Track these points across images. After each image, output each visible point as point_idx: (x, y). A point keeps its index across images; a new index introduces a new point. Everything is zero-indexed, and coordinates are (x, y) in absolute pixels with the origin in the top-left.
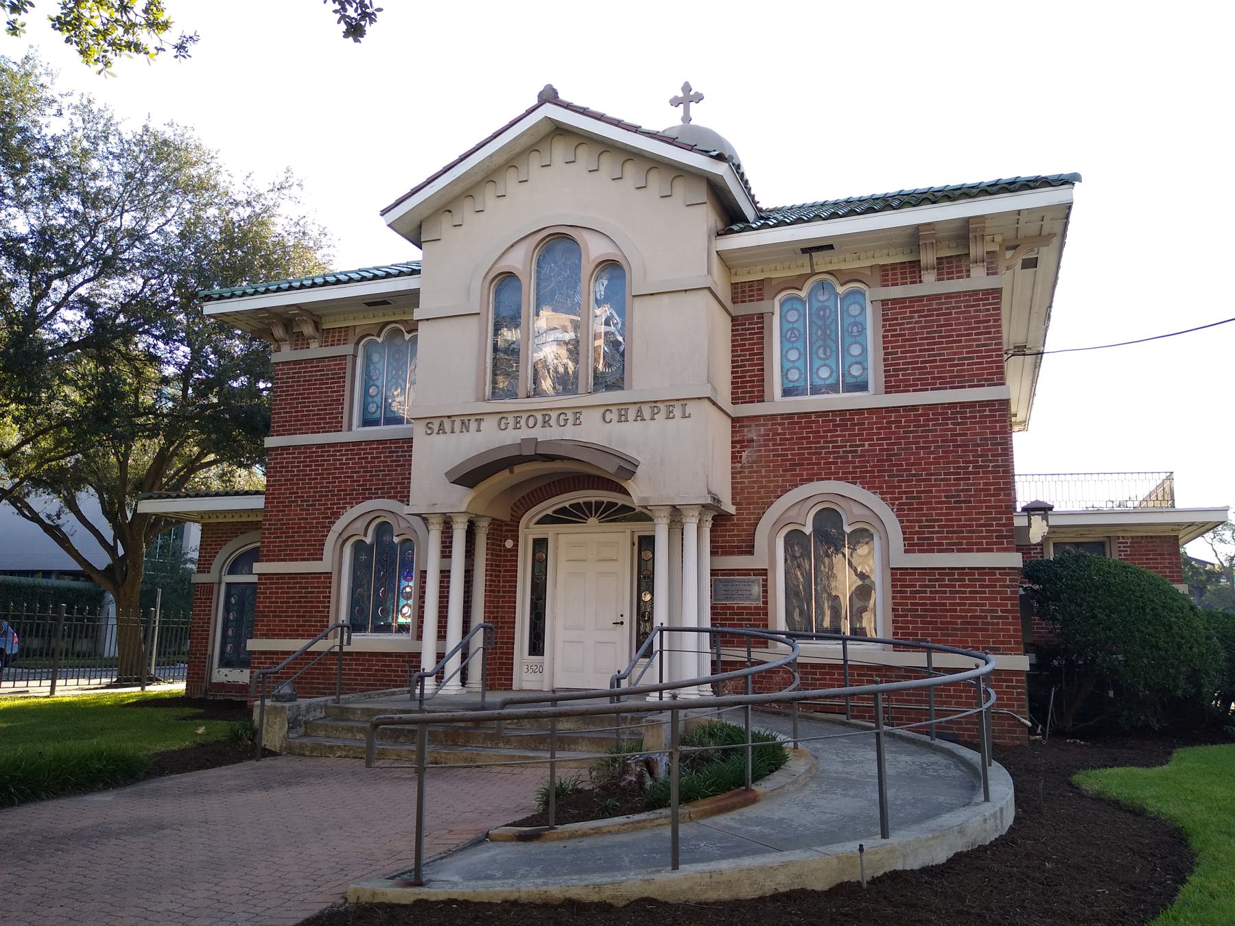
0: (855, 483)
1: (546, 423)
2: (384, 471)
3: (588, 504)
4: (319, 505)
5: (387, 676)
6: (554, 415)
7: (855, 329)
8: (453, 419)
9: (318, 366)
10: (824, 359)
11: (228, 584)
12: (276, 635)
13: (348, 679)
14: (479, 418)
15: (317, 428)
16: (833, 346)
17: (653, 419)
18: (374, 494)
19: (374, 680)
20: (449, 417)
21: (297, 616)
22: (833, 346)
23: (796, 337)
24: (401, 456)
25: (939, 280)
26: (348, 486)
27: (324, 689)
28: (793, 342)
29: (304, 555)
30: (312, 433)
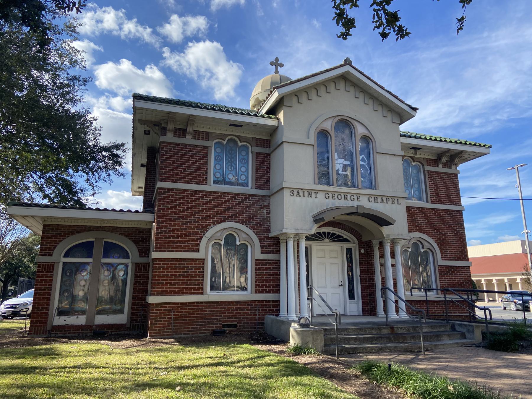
0: (243, 224)
1: (346, 199)
2: (232, 208)
3: (324, 233)
4: (194, 222)
5: (239, 313)
6: (349, 195)
7: (243, 161)
8: (303, 190)
9: (190, 149)
10: (231, 171)
11: (64, 263)
12: (168, 293)
13: (216, 316)
14: (317, 192)
15: (191, 181)
16: (410, 183)
17: (387, 203)
18: (227, 219)
19: (232, 316)
20: (302, 189)
21: (182, 283)
22: (410, 183)
23: (219, 159)
24: (241, 202)
25: (174, 137)
26: (212, 214)
27: (201, 322)
28: (218, 161)
29: (186, 249)
30: (187, 183)
